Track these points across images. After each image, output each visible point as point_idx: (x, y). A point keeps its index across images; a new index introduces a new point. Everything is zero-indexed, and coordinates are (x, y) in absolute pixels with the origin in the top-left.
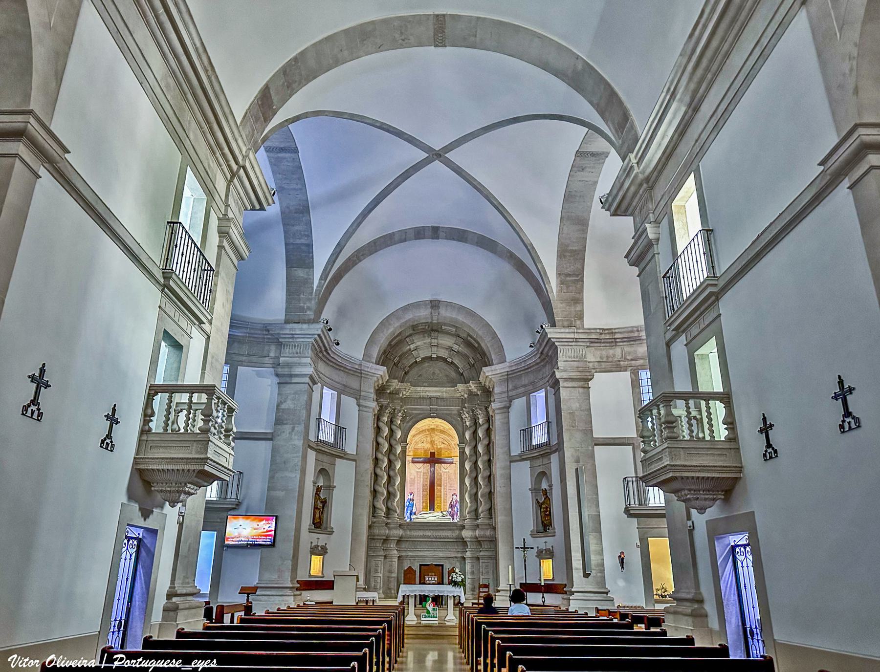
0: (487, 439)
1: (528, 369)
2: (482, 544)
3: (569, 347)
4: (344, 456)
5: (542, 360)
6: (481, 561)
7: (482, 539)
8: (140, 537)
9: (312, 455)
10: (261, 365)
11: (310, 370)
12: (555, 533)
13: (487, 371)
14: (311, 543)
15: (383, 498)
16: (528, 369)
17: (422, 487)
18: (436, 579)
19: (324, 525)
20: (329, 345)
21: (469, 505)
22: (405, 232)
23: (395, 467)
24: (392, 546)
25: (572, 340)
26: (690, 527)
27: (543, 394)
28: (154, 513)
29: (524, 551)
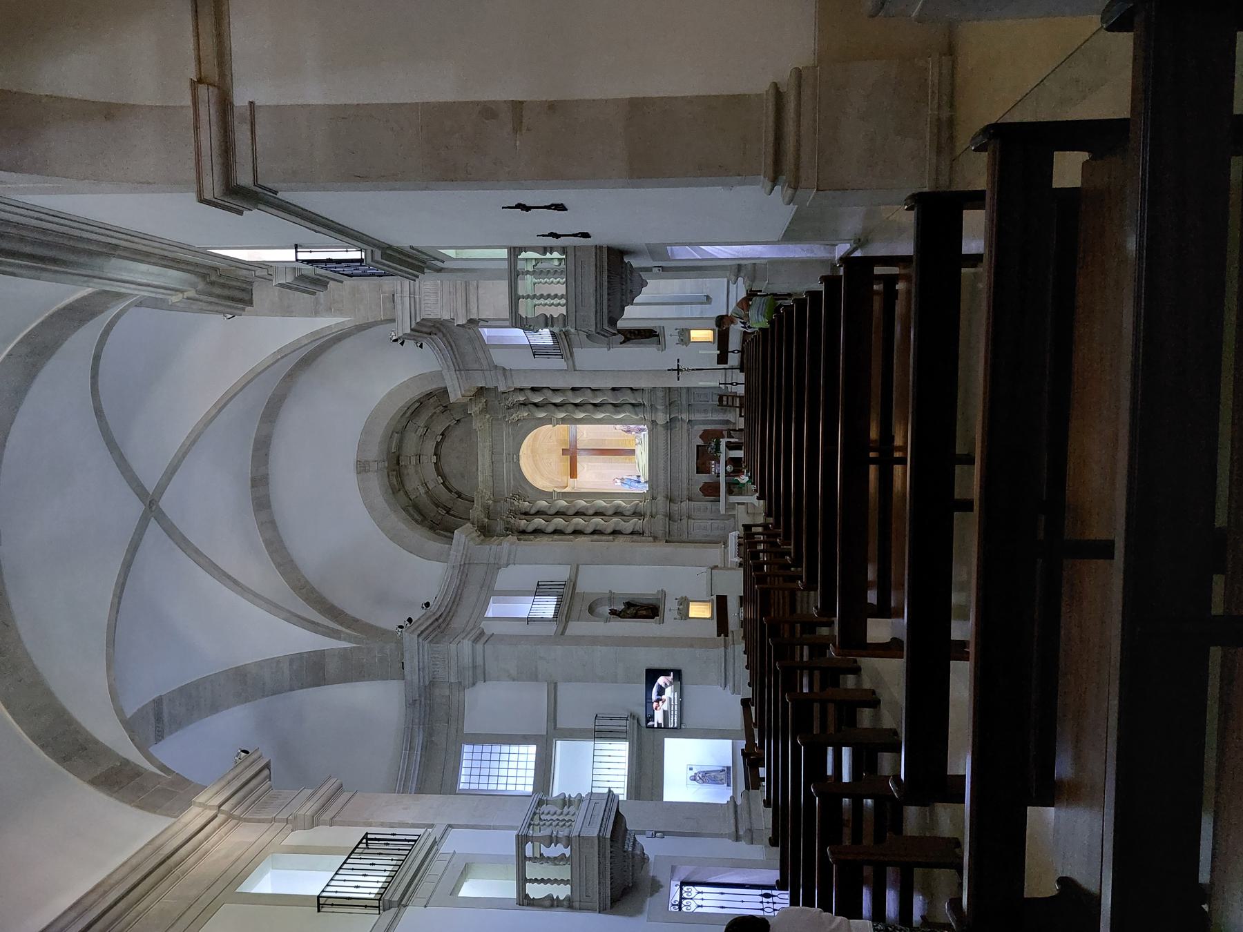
0: (545, 391)
1: (451, 346)
3: (422, 302)
4: (572, 583)
5: (440, 331)
6: (692, 402)
8: (679, 883)
9: (575, 628)
10: (460, 705)
11: (467, 644)
12: (660, 327)
13: (455, 396)
14: (675, 619)
16: (451, 346)
18: (713, 462)
19: (654, 602)
20: (430, 617)
22: (261, 525)
23: (584, 507)
25: (412, 300)
26: (659, 270)
27: (485, 329)
28: (655, 875)
29: (682, 370)
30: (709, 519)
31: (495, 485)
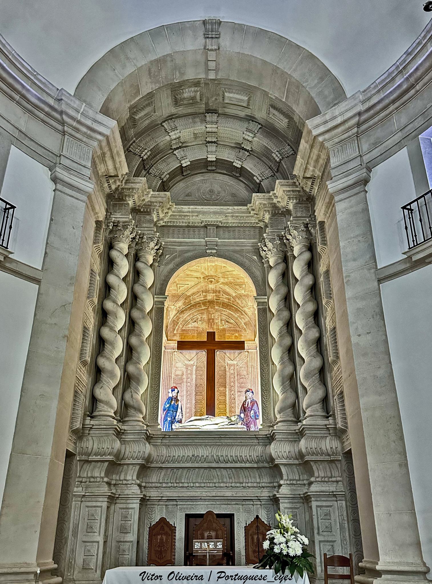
2: (314, 468)
6: (314, 504)
7: (314, 458)
15: (113, 384)
17: (194, 388)
18: (220, 546)
21: (281, 397)
24: (129, 477)
30: (106, 536)
31: (176, 229)
